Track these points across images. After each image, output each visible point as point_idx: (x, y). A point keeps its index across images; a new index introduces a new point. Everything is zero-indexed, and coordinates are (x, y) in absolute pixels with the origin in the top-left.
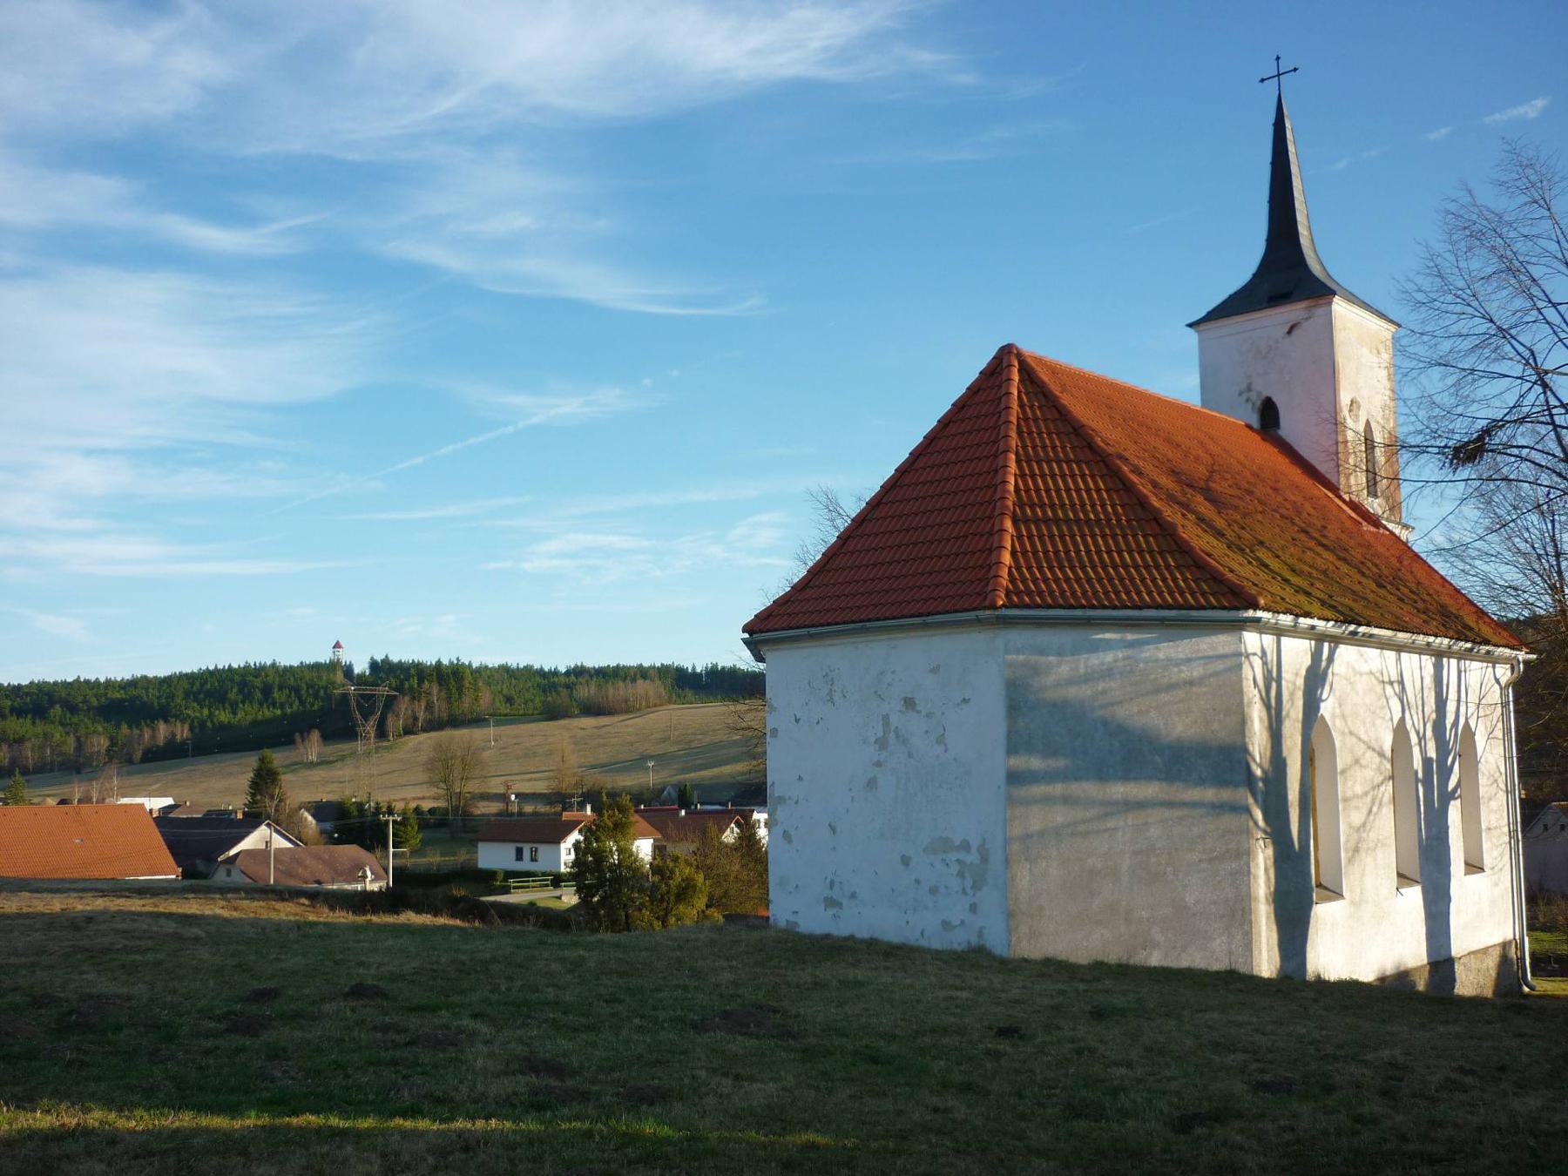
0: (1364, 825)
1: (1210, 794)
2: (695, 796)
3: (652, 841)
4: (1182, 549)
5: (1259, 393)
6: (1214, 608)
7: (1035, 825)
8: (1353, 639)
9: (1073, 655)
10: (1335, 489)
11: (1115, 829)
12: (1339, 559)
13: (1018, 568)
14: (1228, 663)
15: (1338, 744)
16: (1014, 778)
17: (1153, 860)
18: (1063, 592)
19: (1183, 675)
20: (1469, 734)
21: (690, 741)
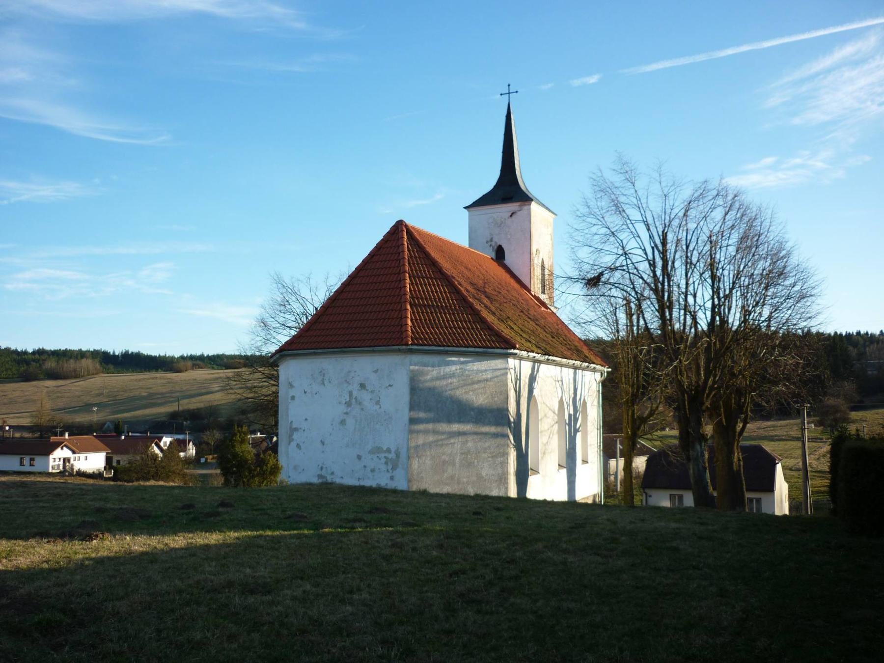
0: (547, 443)
1: (493, 429)
2: (126, 428)
3: (105, 454)
4: (483, 321)
5: (496, 243)
6: (498, 348)
7: (421, 441)
8: (548, 362)
9: (439, 367)
10: (529, 291)
11: (455, 443)
12: (536, 324)
13: (415, 327)
14: (503, 372)
15: (539, 408)
16: (412, 421)
17: (469, 456)
18: (435, 339)
19: (484, 377)
20: (585, 403)
21: (116, 396)
